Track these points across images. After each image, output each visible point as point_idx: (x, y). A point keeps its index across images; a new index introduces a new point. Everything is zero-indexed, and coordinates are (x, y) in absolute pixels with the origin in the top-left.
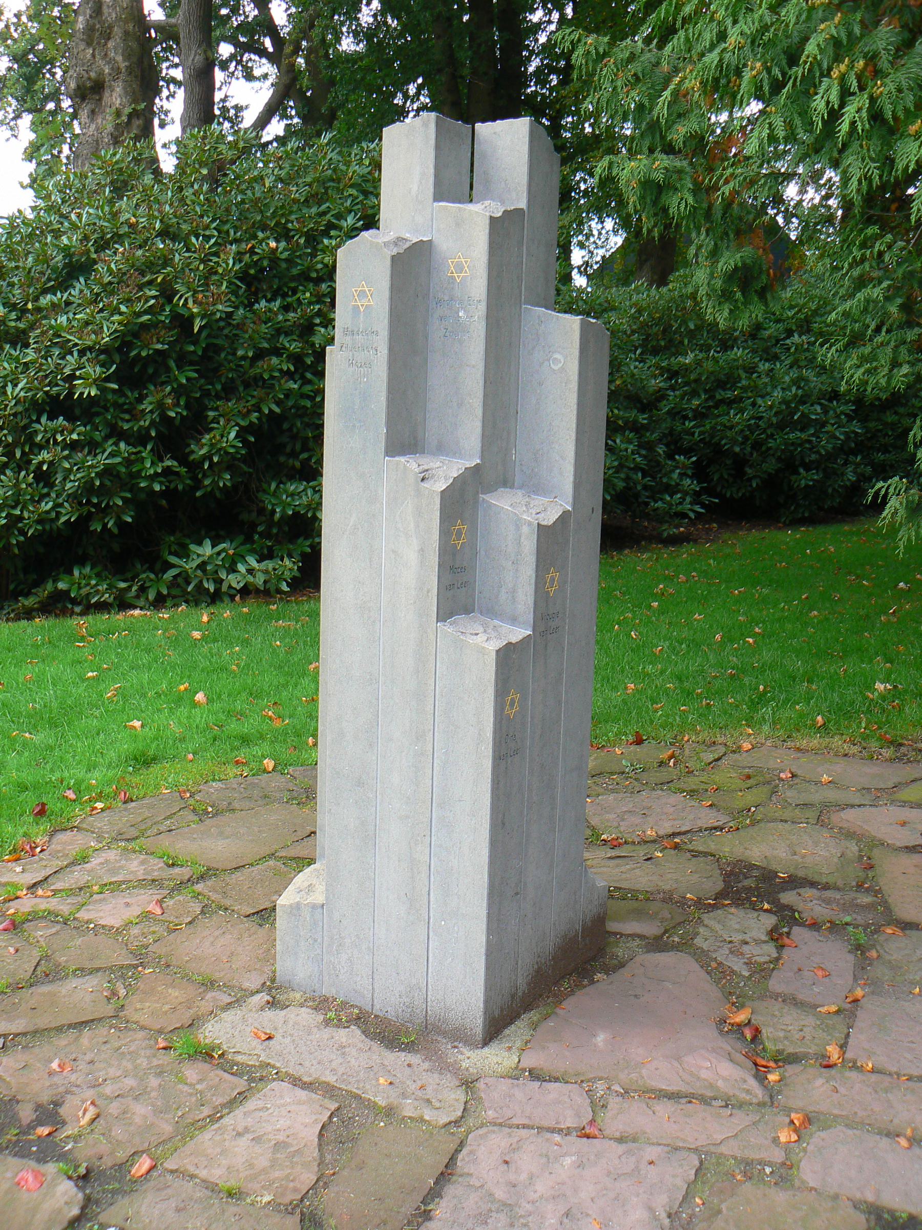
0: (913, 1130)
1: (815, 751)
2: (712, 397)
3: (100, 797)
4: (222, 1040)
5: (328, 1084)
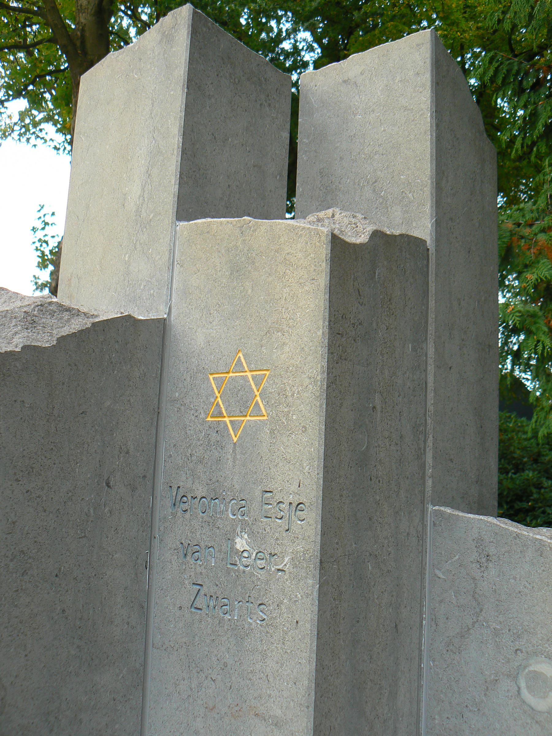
2: (512, 507)
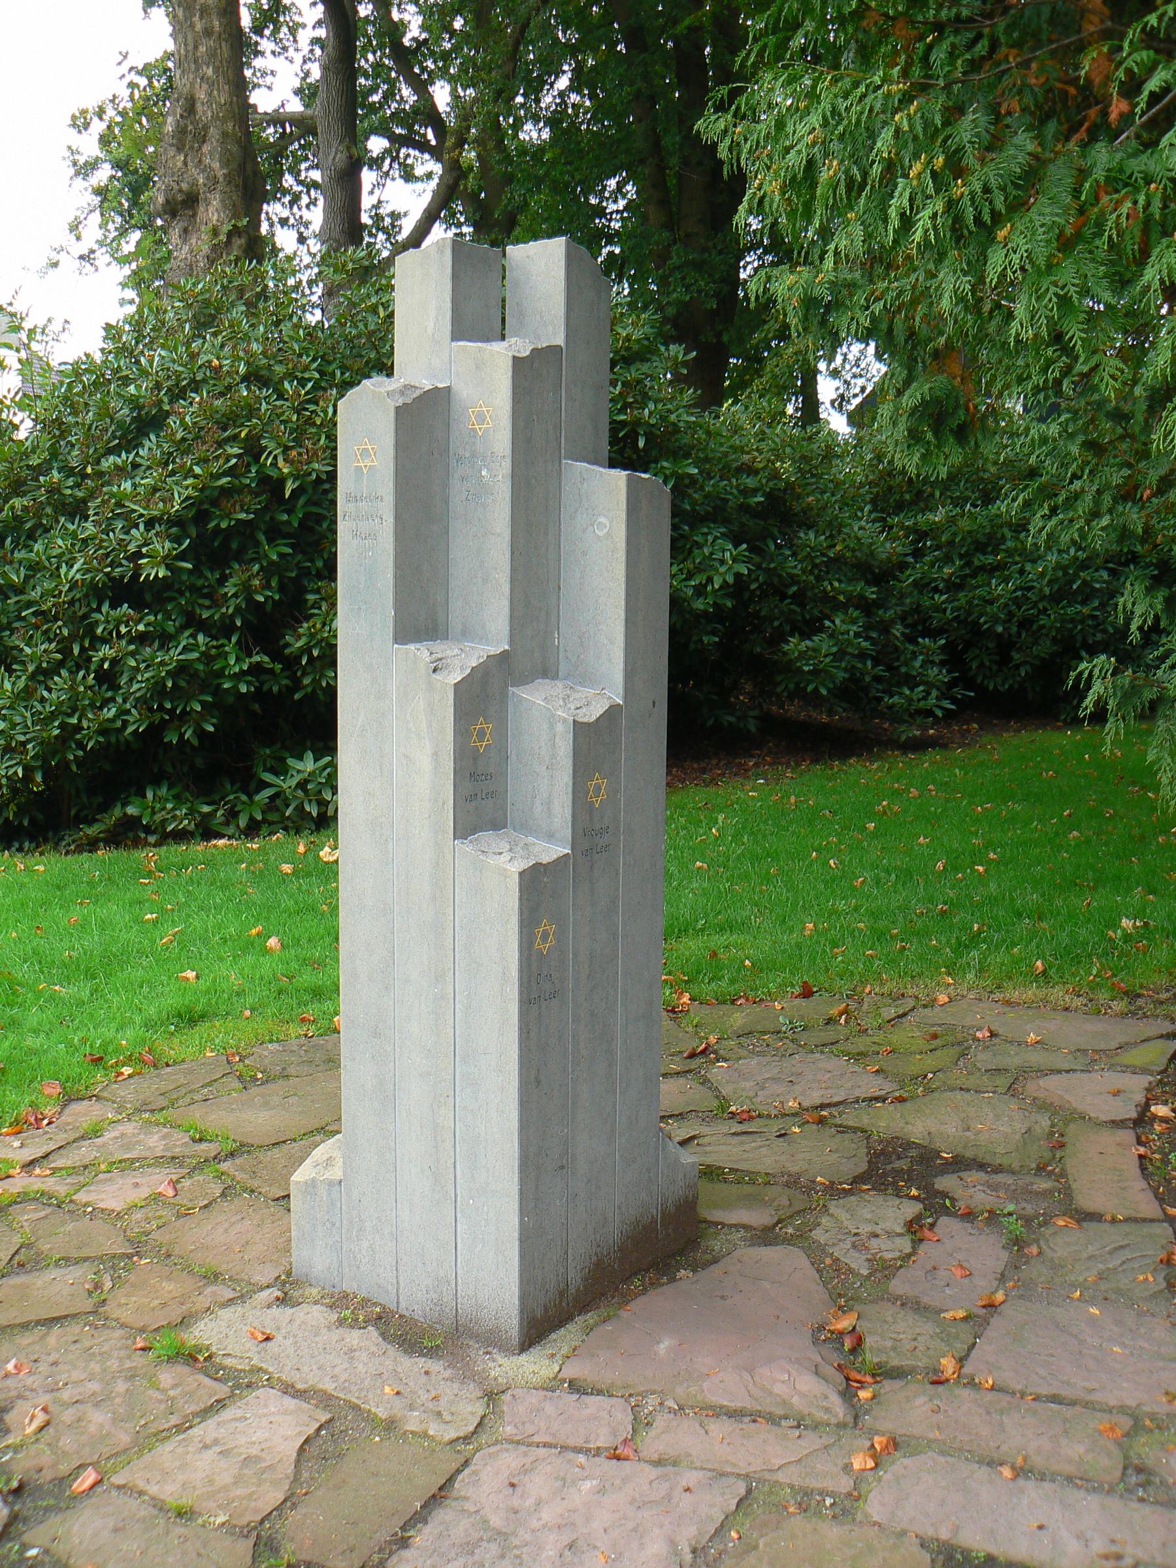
0: (1025, 1459)
1: (1028, 1005)
2: (969, 564)
3: (129, 1060)
4: (214, 1340)
5: (325, 1392)
